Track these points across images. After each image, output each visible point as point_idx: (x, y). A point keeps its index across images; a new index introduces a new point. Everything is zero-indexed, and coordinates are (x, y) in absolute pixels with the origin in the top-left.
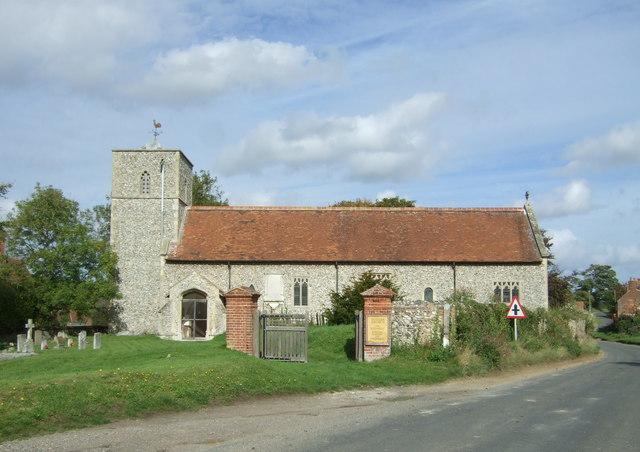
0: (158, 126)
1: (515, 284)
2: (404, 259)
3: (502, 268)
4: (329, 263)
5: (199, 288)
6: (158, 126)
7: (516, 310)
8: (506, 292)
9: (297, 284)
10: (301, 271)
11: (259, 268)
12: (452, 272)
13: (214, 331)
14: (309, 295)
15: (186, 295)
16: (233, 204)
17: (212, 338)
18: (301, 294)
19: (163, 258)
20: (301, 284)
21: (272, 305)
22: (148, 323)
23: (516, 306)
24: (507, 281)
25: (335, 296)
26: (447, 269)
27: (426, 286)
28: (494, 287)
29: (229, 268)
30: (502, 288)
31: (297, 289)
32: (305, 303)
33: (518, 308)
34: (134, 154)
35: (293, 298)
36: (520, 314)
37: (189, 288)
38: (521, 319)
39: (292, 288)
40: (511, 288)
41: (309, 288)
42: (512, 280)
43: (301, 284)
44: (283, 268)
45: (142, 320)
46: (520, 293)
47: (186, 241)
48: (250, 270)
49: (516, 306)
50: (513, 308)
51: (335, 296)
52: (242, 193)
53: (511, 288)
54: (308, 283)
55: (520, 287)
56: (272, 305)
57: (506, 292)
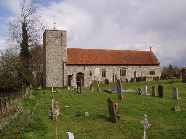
0: (55, 23)
2: (129, 64)
4: (80, 65)
5: (81, 72)
6: (55, 23)
9: (103, 71)
12: (140, 69)
13: (86, 85)
14: (106, 74)
15: (78, 74)
17: (86, 87)
21: (96, 77)
22: (59, 83)
25: (170, 66)
26: (112, 66)
28: (149, 71)
29: (84, 66)
31: (103, 72)
32: (105, 76)
34: (53, 31)
37: (79, 72)
39: (102, 72)
41: (106, 72)
43: (104, 71)
44: (99, 67)
45: (57, 82)
48: (90, 67)
51: (170, 66)
54: (106, 71)
56: (96, 77)
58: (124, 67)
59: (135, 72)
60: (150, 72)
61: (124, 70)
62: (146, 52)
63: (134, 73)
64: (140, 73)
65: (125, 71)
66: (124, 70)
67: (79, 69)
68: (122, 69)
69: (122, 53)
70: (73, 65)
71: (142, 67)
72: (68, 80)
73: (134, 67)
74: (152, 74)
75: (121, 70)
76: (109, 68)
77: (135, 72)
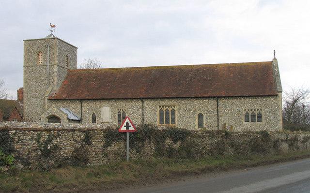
1: (259, 110)
3: (250, 100)
5: (56, 114)
7: (127, 126)
8: (253, 116)
10: (121, 104)
11: (97, 103)
16: (21, 84)
18: (121, 117)
19: (46, 98)
20: (122, 112)
23: (127, 123)
24: (253, 108)
26: (213, 102)
27: (199, 112)
28: (244, 113)
30: (250, 113)
31: (119, 115)
33: (130, 124)
35: (117, 120)
36: (131, 128)
38: (131, 133)
40: (256, 113)
42: (257, 108)
44: (112, 102)
46: (263, 115)
47: (63, 87)
49: (127, 123)
50: (125, 124)
52: (89, 56)
53: (256, 113)
55: (263, 112)
57: (253, 116)
58: (170, 102)
59: (201, 116)
60: (247, 116)
61: (170, 109)
62: (210, 68)
63: (197, 117)
64: (215, 118)
65: (173, 113)
66: (170, 109)
67: (50, 109)
68: (164, 109)
69: (180, 69)
70: (233, 98)
71: (222, 102)
72: (293, 183)
73: (198, 103)
74: (253, 121)
75: (161, 111)
76: (133, 106)
77: (201, 116)
